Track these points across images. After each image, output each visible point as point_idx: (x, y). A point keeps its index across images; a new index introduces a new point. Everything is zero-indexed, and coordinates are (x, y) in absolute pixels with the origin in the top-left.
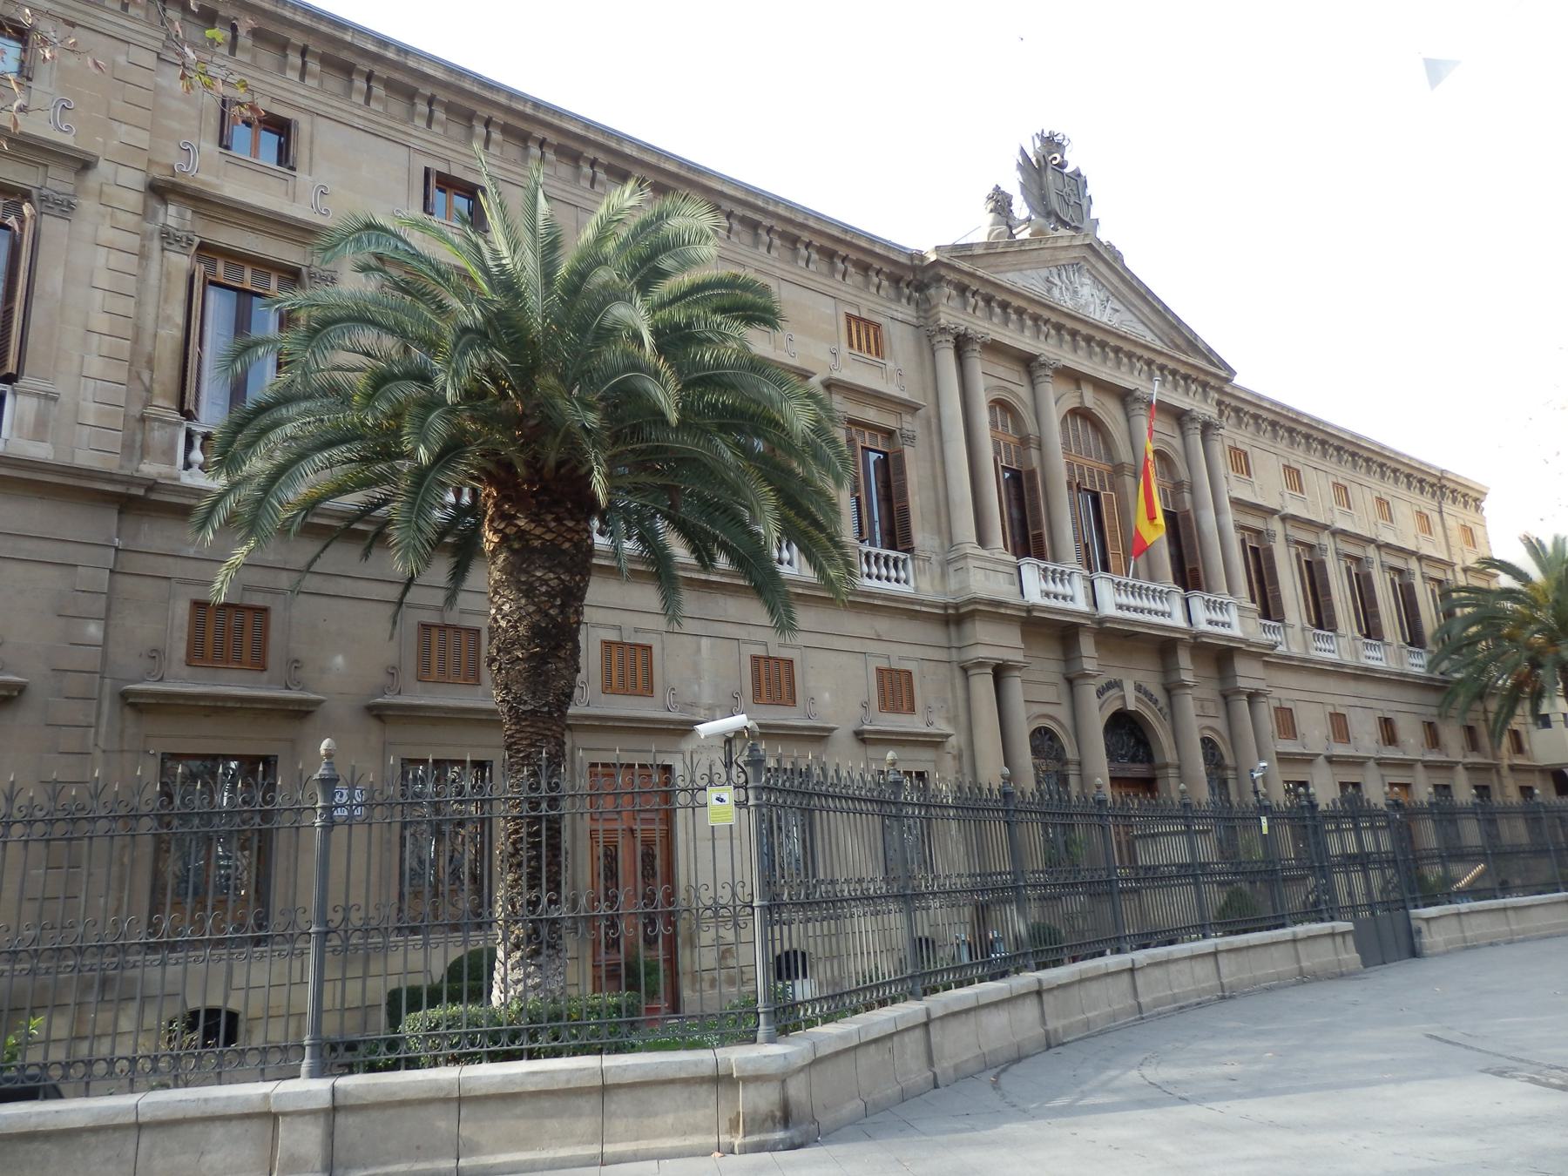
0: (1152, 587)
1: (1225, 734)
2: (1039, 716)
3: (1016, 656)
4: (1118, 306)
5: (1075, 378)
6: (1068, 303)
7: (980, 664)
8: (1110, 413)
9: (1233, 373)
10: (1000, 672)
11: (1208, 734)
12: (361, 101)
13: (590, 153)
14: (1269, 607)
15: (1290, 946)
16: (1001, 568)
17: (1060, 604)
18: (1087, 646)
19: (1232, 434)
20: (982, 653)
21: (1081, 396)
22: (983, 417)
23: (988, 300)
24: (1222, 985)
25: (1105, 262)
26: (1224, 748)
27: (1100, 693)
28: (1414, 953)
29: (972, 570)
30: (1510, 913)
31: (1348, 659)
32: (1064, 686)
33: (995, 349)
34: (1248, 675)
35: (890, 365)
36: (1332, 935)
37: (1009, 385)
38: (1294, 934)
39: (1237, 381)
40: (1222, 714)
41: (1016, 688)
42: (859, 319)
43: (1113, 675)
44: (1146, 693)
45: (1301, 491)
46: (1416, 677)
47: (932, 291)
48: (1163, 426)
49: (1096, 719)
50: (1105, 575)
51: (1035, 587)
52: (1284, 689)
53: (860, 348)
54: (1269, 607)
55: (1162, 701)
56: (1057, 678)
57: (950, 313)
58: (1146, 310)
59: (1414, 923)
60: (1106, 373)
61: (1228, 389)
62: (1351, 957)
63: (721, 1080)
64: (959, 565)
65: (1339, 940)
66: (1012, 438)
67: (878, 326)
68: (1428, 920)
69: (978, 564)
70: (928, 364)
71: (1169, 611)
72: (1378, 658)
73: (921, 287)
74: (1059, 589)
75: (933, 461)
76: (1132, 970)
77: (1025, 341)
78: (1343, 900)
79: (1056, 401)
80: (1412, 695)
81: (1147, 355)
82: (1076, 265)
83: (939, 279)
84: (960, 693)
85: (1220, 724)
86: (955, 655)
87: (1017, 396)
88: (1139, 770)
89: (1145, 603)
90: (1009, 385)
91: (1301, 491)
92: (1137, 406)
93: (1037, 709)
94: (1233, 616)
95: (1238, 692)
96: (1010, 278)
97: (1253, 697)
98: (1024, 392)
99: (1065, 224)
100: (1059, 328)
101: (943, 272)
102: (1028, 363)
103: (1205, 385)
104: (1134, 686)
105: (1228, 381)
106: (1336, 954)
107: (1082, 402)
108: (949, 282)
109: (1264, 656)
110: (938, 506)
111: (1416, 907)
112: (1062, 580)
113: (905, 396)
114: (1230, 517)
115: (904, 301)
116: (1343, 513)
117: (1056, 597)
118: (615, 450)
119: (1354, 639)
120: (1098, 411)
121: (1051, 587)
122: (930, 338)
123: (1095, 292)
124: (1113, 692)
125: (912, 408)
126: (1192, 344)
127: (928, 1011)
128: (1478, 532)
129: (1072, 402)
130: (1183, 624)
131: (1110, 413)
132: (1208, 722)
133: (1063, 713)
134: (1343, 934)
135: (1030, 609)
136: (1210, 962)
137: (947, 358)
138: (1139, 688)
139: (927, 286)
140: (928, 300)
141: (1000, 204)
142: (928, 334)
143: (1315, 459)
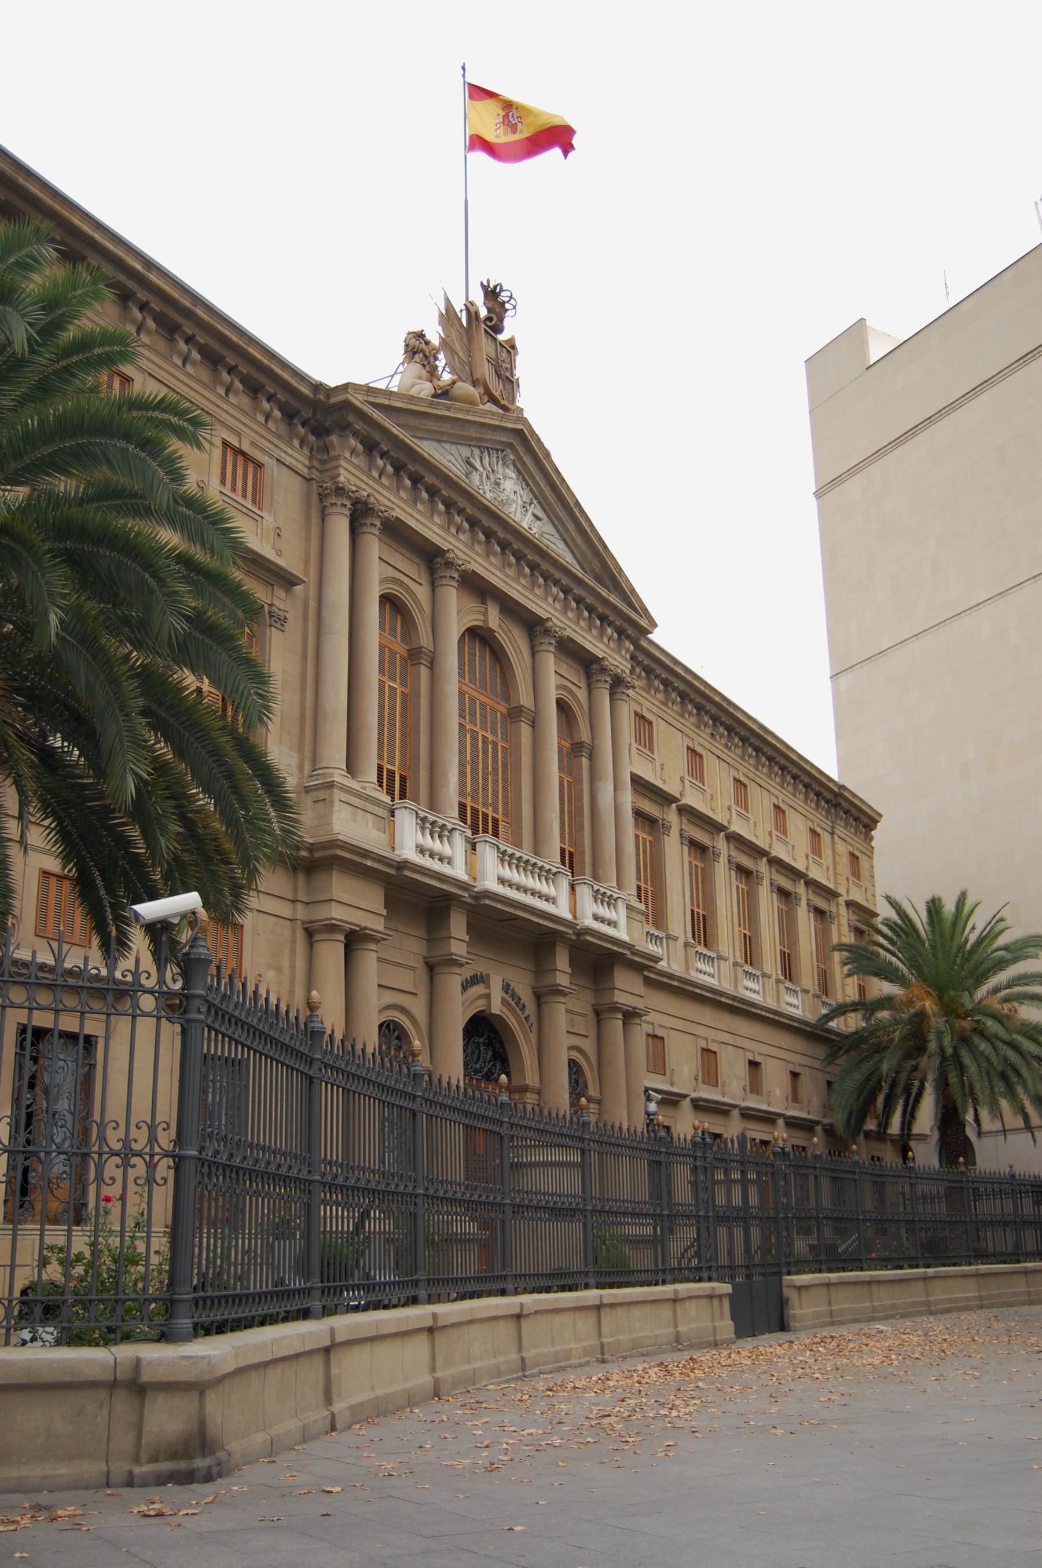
0: (540, 864)
2: (389, 1007)
3: (376, 924)
4: (540, 513)
5: (477, 587)
6: (488, 495)
7: (332, 928)
8: (514, 642)
9: (654, 625)
10: (354, 941)
11: (576, 1055)
12: (223, 393)
13: (189, 328)
15: (669, 1305)
16: (370, 807)
17: (436, 866)
18: (458, 926)
19: (642, 699)
20: (337, 913)
21: (485, 614)
22: (372, 611)
23: (398, 468)
24: (602, 1345)
25: (524, 449)
26: (590, 1076)
27: (465, 987)
29: (337, 806)
30: (874, 1287)
31: (726, 986)
32: (422, 972)
33: (396, 533)
34: (627, 989)
35: (268, 518)
37: (406, 580)
38: (676, 1291)
39: (655, 636)
40: (592, 1033)
41: (369, 960)
42: (239, 452)
43: (479, 967)
44: (513, 995)
45: (747, 810)
46: (792, 1018)
47: (334, 438)
48: (574, 676)
49: (457, 1012)
50: (493, 840)
51: (409, 841)
52: (662, 1013)
53: (234, 489)
55: (531, 1008)
56: (418, 963)
57: (352, 472)
58: (571, 527)
59: (787, 1292)
60: (517, 590)
61: (644, 644)
63: (136, 1387)
64: (321, 795)
65: (716, 1302)
66: (401, 649)
67: (259, 465)
68: (799, 1289)
69: (345, 797)
70: (315, 530)
71: (558, 900)
72: (753, 991)
73: (320, 431)
74: (437, 846)
75: (304, 656)
76: (518, 1317)
77: (431, 528)
78: (724, 1260)
79: (457, 613)
80: (785, 1040)
81: (565, 581)
82: (498, 449)
83: (344, 428)
84: (301, 964)
85: (588, 1045)
86: (301, 913)
87: (574, 696)
89: (531, 882)
90: (406, 580)
91: (747, 810)
92: (547, 640)
93: (390, 998)
94: (620, 914)
95: (614, 1008)
96: (428, 448)
97: (630, 1016)
98: (422, 592)
99: (493, 400)
100: (473, 523)
101: (351, 418)
102: (431, 558)
103: (621, 632)
104: (501, 986)
105: (646, 632)
106: (713, 1320)
107: (486, 621)
108: (356, 434)
109: (643, 966)
110: (303, 717)
111: (789, 1273)
112: (440, 837)
113: (281, 562)
114: (628, 798)
115: (296, 442)
116: (739, 814)
117: (432, 856)
118: (490, 818)
119: (736, 964)
120: (502, 637)
121: (428, 842)
122: (322, 497)
123: (518, 489)
124: (478, 989)
125: (287, 581)
126: (609, 573)
127: (332, 1331)
128: (864, 862)
129: (474, 620)
130: (568, 916)
131: (514, 642)
132: (576, 1041)
133: (418, 1007)
134: (720, 1297)
135: (404, 865)
136: (592, 1316)
137: (340, 526)
138: (506, 988)
139: (328, 432)
140: (326, 449)
141: (417, 348)
142: (323, 495)
143: (672, 712)
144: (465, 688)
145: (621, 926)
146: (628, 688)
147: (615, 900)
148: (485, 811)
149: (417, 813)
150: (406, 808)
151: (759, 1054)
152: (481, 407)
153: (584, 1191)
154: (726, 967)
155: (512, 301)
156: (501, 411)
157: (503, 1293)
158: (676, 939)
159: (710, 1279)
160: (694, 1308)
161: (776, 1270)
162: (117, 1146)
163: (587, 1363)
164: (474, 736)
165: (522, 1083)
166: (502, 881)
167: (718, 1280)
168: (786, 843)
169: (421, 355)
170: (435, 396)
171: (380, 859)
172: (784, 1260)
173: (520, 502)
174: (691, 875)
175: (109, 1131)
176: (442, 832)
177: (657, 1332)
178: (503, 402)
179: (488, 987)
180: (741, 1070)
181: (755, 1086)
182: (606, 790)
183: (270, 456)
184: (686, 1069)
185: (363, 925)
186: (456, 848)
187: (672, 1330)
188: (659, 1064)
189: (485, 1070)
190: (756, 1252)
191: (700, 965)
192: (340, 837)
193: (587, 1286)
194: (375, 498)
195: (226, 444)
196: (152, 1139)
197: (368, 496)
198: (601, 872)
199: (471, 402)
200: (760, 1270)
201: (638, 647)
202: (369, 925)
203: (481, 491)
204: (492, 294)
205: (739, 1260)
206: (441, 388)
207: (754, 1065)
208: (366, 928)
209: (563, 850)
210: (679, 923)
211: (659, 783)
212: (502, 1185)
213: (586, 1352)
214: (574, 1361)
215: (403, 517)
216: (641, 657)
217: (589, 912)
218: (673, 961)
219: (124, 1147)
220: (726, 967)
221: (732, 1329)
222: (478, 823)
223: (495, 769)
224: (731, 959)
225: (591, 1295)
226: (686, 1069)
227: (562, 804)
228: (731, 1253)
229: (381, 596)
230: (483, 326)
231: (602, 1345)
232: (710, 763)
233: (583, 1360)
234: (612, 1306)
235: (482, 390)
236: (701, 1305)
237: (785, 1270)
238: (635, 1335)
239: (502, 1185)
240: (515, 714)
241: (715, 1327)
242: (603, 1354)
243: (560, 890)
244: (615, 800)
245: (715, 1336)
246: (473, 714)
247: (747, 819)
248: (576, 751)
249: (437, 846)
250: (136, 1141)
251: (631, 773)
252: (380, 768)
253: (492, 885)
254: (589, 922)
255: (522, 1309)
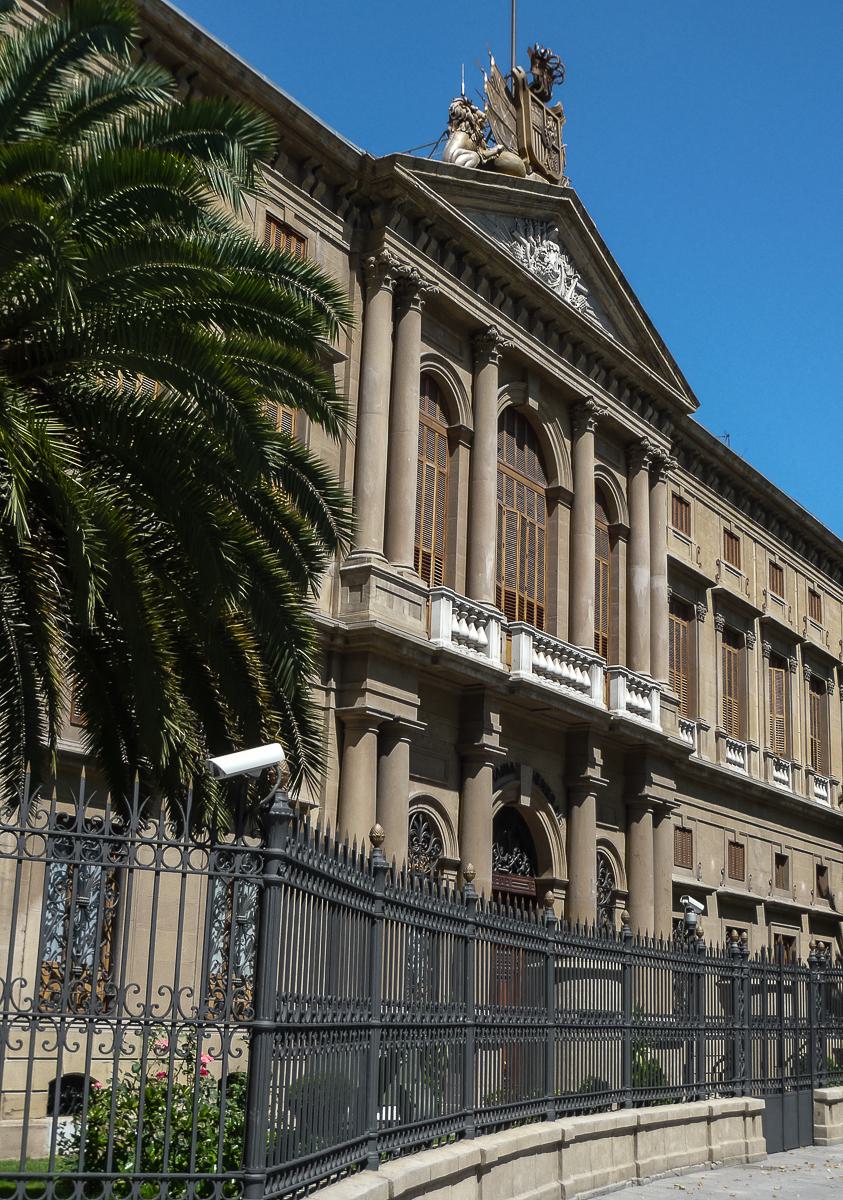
1: (622, 852)
14: (687, 703)
17: (471, 654)
19: (678, 481)
24: (638, 1167)
28: (814, 1143)
29: (374, 591)
34: (660, 788)
36: (744, 1114)
50: (533, 628)
54: (687, 703)
61: (684, 423)
62: (758, 1141)
69: (383, 583)
74: (473, 633)
88: (523, 885)
94: (654, 704)
97: (661, 811)
99: (538, 169)
111: (821, 1086)
116: (774, 599)
118: (525, 602)
121: (463, 628)
126: (651, 349)
130: (603, 707)
134: (753, 1114)
135: (440, 655)
144: (503, 468)
145: (657, 720)
146: (667, 469)
147: (650, 690)
148: (531, 600)
149: (454, 600)
150: (443, 595)
151: (787, 847)
152: (527, 177)
153: (623, 1008)
154: (757, 757)
155: (560, 69)
156: (546, 182)
157: (544, 1118)
158: (707, 729)
159: (743, 1094)
160: (727, 1124)
161: (808, 1082)
162: (137, 1012)
163: (623, 1187)
164: (511, 516)
165: (550, 877)
166: (537, 670)
167: (750, 1095)
168: (820, 629)
169: (468, 123)
170: (481, 166)
171: (416, 647)
172: (815, 1073)
173: (564, 276)
174: (724, 661)
175: (129, 994)
176: (479, 620)
177: (691, 1151)
178: (548, 172)
179: (518, 778)
180: (768, 864)
181: (782, 881)
182: (643, 576)
183: (314, 229)
184: (713, 862)
185: (397, 715)
186: (493, 636)
187: (705, 1148)
188: (685, 858)
189: (512, 861)
190: (789, 1060)
191: (731, 755)
192: (377, 625)
193: (622, 1106)
194: (419, 272)
195: (270, 218)
196: (175, 1005)
197: (413, 270)
198: (635, 660)
199: (515, 170)
200: (792, 1083)
201: (678, 426)
202: (402, 716)
203: (525, 265)
204: (539, 59)
205: (772, 1073)
206: (486, 158)
207: (781, 860)
208: (399, 719)
209: (597, 636)
210: (711, 710)
211: (695, 567)
212: (546, 1006)
213: (622, 1175)
214: (611, 1185)
215: (447, 292)
216: (681, 435)
217: (623, 703)
218: (706, 754)
219: (144, 1013)
220: (757, 757)
221: (764, 1146)
222: (521, 611)
223: (532, 552)
224: (762, 750)
225: (628, 1116)
226: (713, 862)
227: (597, 589)
228: (764, 1066)
229: (422, 373)
230: (530, 93)
231: (638, 1167)
232: (747, 546)
233: (620, 1184)
234: (649, 1127)
235: (528, 160)
236: (731, 1123)
237: (816, 1083)
238: (671, 1155)
239: (546, 1006)
240: (556, 497)
241: (747, 1144)
242: (638, 1176)
243: (596, 680)
244: (651, 584)
245: (747, 1152)
246: (510, 494)
247: (782, 604)
248: (617, 534)
249: (473, 633)
250: (157, 1007)
251: (671, 560)
252: (417, 551)
253: (527, 675)
254: (623, 713)
255: (563, 1136)
